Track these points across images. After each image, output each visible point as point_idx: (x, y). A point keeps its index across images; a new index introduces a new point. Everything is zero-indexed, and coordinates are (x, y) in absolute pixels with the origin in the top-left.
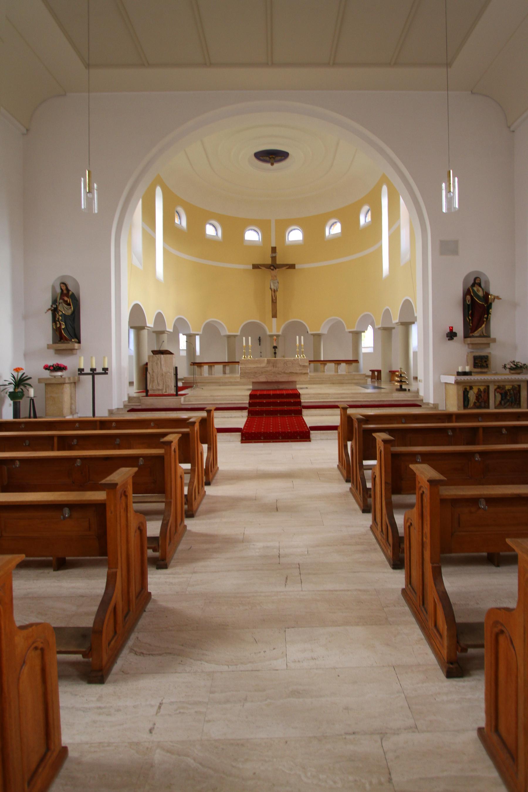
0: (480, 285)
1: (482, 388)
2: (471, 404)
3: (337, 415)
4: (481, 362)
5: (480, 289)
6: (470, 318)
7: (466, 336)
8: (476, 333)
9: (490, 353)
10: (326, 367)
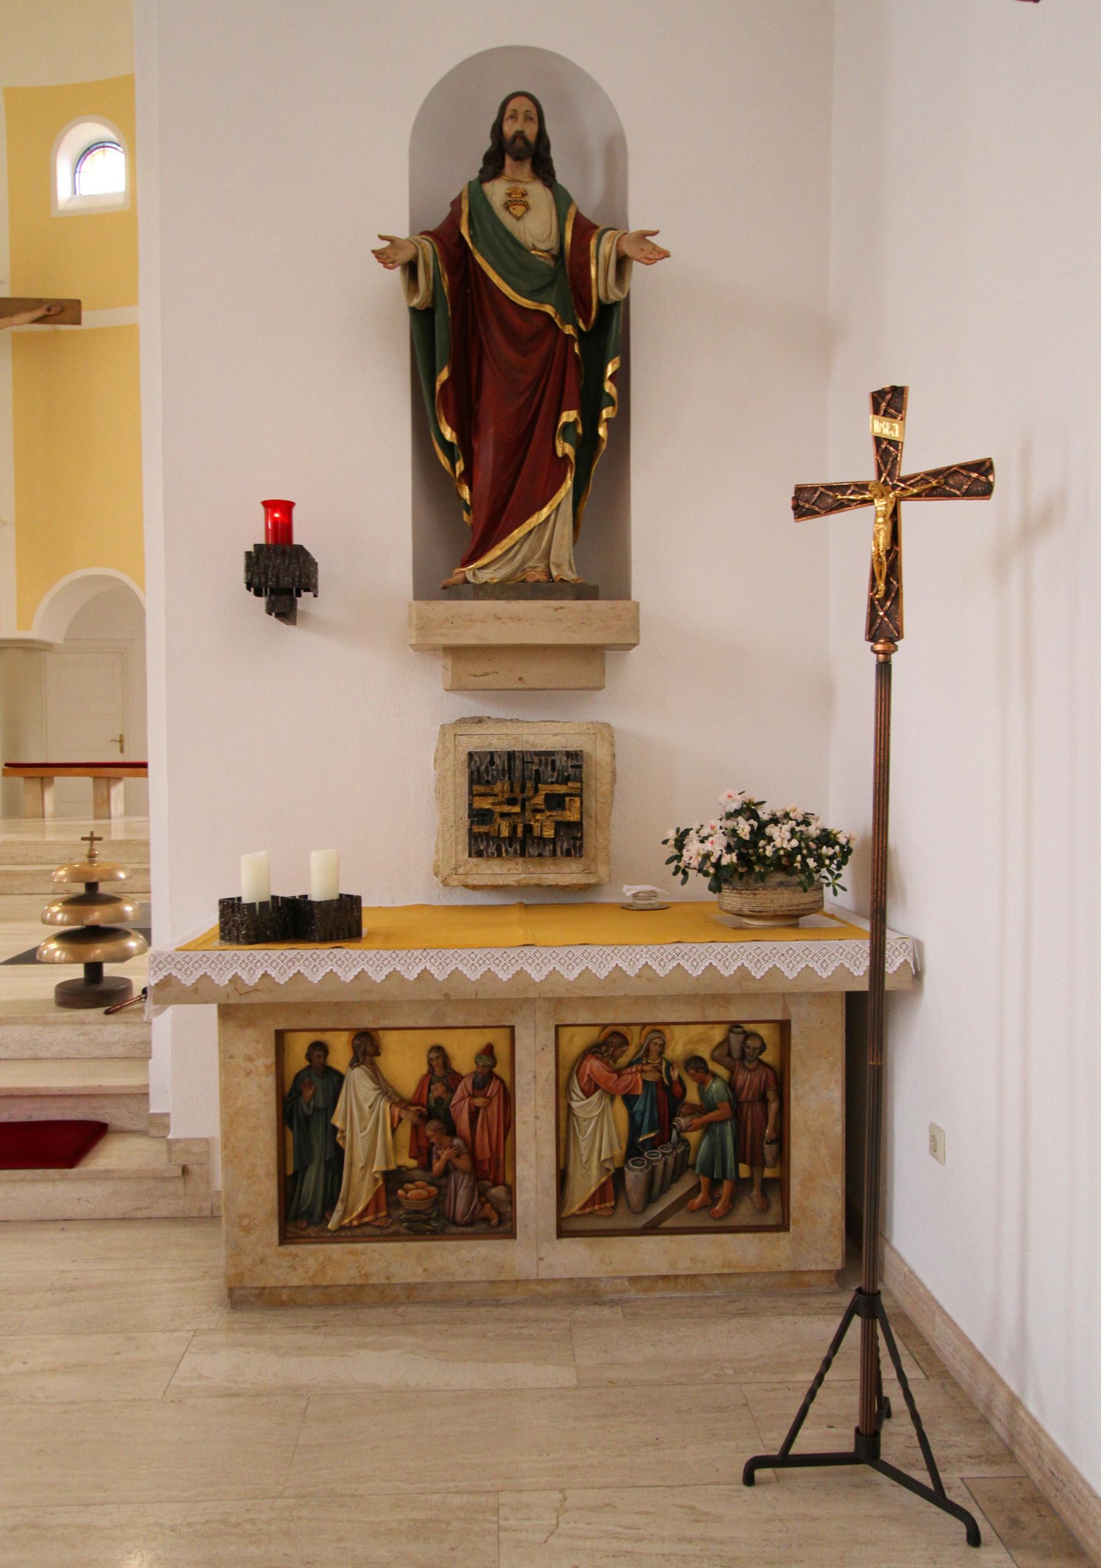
0: (538, 158)
1: (463, 1055)
2: (360, 1188)
3: (371, 909)
4: (91, 856)
5: (538, 193)
6: (449, 434)
7: (438, 583)
8: (491, 568)
9: (606, 732)
10: (49, 796)
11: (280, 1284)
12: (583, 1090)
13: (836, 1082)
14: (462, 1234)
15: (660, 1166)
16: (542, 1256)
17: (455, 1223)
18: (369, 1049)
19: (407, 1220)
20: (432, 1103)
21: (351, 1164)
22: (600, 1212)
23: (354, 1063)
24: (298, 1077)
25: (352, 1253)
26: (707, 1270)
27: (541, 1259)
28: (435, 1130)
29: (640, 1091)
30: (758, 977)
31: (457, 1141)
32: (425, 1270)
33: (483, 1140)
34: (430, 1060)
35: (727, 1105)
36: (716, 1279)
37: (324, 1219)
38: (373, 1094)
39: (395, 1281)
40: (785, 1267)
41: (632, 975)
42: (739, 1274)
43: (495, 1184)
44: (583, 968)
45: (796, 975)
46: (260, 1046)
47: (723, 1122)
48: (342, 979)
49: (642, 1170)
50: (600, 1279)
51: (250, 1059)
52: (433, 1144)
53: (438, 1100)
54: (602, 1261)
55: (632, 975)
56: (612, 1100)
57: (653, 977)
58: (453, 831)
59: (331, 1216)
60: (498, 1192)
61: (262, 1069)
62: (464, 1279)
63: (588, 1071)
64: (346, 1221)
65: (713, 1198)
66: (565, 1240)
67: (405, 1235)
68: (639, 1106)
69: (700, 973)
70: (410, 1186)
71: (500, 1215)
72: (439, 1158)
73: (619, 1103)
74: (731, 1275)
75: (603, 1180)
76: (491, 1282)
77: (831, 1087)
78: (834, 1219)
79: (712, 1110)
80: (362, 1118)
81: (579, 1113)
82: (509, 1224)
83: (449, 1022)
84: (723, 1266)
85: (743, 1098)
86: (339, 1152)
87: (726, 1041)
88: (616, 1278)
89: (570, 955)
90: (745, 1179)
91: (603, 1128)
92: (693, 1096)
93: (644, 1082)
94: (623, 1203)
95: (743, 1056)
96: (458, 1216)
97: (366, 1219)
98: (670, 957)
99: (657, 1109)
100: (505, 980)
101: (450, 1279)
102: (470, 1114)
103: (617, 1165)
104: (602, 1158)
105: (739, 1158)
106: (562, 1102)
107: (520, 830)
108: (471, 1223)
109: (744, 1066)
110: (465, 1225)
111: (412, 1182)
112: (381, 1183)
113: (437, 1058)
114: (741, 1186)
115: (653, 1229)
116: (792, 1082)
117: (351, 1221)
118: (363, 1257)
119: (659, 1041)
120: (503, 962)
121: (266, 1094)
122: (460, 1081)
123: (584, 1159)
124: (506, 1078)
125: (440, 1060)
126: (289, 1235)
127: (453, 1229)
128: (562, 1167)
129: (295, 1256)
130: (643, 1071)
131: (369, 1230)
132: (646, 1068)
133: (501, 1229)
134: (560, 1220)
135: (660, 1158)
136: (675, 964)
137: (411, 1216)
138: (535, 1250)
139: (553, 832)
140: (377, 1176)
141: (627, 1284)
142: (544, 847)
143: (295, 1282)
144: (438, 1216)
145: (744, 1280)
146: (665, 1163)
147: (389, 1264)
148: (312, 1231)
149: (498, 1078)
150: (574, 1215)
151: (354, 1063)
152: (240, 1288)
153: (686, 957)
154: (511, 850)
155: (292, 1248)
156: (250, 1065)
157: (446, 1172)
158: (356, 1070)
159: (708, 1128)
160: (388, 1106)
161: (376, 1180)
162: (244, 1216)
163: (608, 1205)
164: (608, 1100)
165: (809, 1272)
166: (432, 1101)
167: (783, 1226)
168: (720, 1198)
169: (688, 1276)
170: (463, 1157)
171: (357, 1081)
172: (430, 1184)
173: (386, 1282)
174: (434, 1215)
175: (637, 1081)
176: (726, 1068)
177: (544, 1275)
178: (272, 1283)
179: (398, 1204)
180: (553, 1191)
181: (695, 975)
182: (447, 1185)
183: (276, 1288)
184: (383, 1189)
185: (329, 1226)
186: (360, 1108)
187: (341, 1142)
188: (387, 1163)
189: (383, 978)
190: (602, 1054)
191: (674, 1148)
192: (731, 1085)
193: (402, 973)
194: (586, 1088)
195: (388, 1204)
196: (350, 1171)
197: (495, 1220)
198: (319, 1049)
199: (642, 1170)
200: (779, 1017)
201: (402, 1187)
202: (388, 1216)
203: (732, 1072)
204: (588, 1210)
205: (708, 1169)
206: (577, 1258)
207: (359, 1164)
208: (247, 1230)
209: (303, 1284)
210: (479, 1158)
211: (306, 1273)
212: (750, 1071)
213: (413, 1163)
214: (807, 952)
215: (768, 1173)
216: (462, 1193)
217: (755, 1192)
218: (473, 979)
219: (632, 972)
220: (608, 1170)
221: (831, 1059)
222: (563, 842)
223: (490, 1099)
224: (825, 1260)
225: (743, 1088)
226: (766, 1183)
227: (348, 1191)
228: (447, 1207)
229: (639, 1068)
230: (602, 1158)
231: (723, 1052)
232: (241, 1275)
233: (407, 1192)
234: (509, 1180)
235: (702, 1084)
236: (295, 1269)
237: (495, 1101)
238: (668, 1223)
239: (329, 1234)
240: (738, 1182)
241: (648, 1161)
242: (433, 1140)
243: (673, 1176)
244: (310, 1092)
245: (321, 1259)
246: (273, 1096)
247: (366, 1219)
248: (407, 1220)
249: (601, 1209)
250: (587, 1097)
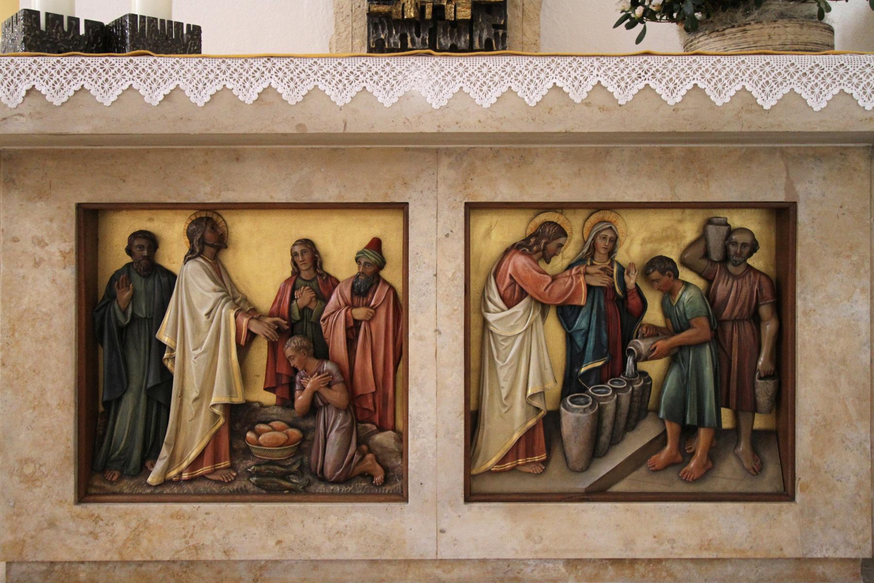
2: (193, 428)
11: (75, 559)
12: (503, 298)
13: (863, 290)
14: (333, 493)
15: (610, 406)
16: (443, 526)
17: (323, 479)
18: (208, 235)
19: (257, 474)
20: (297, 316)
21: (181, 395)
22: (527, 469)
23: (191, 256)
24: (113, 279)
25: (177, 516)
26: (677, 553)
27: (442, 531)
28: (298, 349)
29: (582, 301)
30: (767, 107)
31: (327, 366)
32: (279, 542)
33: (364, 365)
34: (294, 255)
35: (704, 322)
36: (690, 565)
37: (143, 470)
38: (213, 297)
39: (236, 557)
40: (790, 552)
41: (578, 100)
42: (723, 560)
43: (381, 429)
44: (505, 89)
45: (824, 105)
46: (55, 226)
47: (700, 345)
48: (147, 99)
49: (585, 411)
50: (524, 562)
51: (40, 243)
52: (295, 371)
53: (303, 310)
54: (528, 536)
55: (578, 100)
56: (544, 315)
57: (610, 105)
58: (349, 21)
59: (153, 466)
60: (385, 438)
61: (58, 257)
62: (334, 557)
63: (510, 271)
64: (173, 473)
65: (684, 455)
66: (476, 506)
67: (254, 493)
68: (581, 322)
69: (679, 99)
70: (262, 427)
71: (386, 470)
72: (303, 388)
73: (552, 320)
74: (711, 560)
75: (531, 423)
76: (373, 562)
77: (855, 297)
78: (859, 485)
79: (682, 330)
80: (197, 330)
81: (496, 328)
82: (399, 484)
83: (318, 197)
84: (701, 548)
85: (726, 314)
86: (166, 377)
87: (703, 237)
88: (547, 560)
89: (485, 70)
90: (727, 431)
91: (531, 355)
92: (654, 315)
93: (589, 288)
94: (557, 456)
95: (726, 258)
96: (328, 468)
97: (200, 472)
98: (634, 75)
99: (603, 326)
100: (387, 104)
101: (313, 556)
102: (348, 329)
103: (550, 407)
104: (530, 392)
105: (722, 400)
106: (475, 319)
107: (428, 11)
108: (345, 480)
109: (729, 273)
110: (336, 482)
111: (266, 422)
112: (222, 421)
113: (303, 252)
114: (723, 440)
115: (599, 493)
116: (798, 290)
117: (180, 474)
118: (193, 522)
119: (609, 234)
120: (385, 78)
121: (62, 292)
122: (334, 287)
123: (504, 393)
124: (399, 286)
125: (307, 256)
126: (93, 491)
127: (321, 488)
128: (472, 407)
129: (97, 519)
130: (586, 273)
131: (202, 486)
132: (591, 270)
133: (388, 488)
134: (469, 478)
135: (611, 397)
136: (641, 86)
137: (263, 468)
138: (433, 513)
139: (469, 11)
140: (217, 410)
141: (563, 570)
142: (459, 37)
143: (96, 556)
144: (299, 468)
145: (730, 569)
146: (618, 403)
147: (228, 533)
148: (125, 486)
149: (385, 282)
150: (489, 472)
151: (191, 256)
152: (21, 563)
153: (658, 76)
154: (418, 40)
155: (93, 508)
156: (39, 252)
157: (314, 408)
158: (191, 264)
159: (675, 356)
160: (232, 315)
161: (215, 416)
162: (26, 461)
163: (536, 459)
164: (538, 313)
165: (825, 560)
166: (296, 311)
167: (785, 493)
168: (693, 453)
169: (650, 561)
170: (335, 387)
171: (190, 279)
172: (291, 425)
173: (224, 558)
174: (295, 468)
175: (579, 286)
176: (700, 274)
177: (447, 554)
178: (64, 556)
179: (247, 452)
180: (460, 435)
181: (671, 102)
182: (314, 428)
183: (70, 562)
184: (226, 430)
185: (149, 480)
186: (194, 317)
187: (169, 366)
188: (230, 392)
189: (207, 99)
190: (530, 248)
191: (630, 383)
192: (709, 295)
193: (235, 92)
194: (508, 294)
195: (233, 452)
196: (181, 404)
197: (378, 475)
198: (147, 242)
199: (585, 411)
200: (780, 197)
201: (252, 429)
202: (232, 467)
203: (709, 280)
204: (508, 465)
205: (677, 413)
206: (492, 532)
207: (192, 393)
208: (31, 481)
209: (107, 558)
210: (360, 391)
211: (113, 542)
212: (735, 277)
213: (269, 398)
214: (841, 71)
215: (760, 422)
216: (334, 437)
217: (743, 447)
218: (340, 104)
219: (577, 97)
220: (538, 410)
221: (855, 258)
222: (482, 30)
223: (375, 309)
224: (848, 544)
225: (725, 301)
226: (757, 437)
227: (177, 431)
228: (313, 458)
229: (582, 269)
230: (530, 392)
231: (700, 256)
232: (20, 544)
233: (258, 435)
234: (400, 424)
235: (668, 293)
236: (96, 537)
237: (382, 312)
238: (621, 487)
239: (148, 491)
240: (718, 432)
241: (593, 397)
242: (294, 363)
243: (627, 422)
244: (127, 294)
245: (134, 524)
246: (71, 296)
247: (200, 472)
248: (257, 474)
249: (527, 464)
250: (509, 308)
